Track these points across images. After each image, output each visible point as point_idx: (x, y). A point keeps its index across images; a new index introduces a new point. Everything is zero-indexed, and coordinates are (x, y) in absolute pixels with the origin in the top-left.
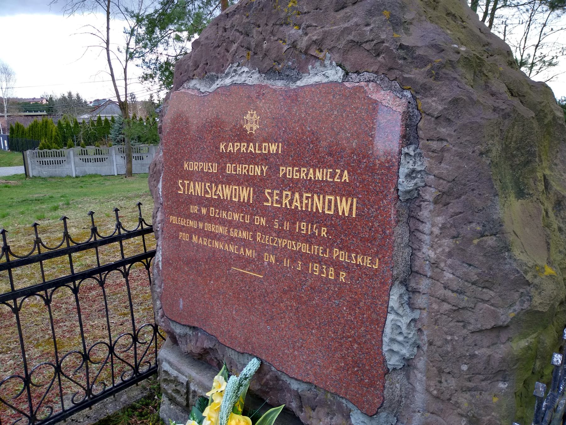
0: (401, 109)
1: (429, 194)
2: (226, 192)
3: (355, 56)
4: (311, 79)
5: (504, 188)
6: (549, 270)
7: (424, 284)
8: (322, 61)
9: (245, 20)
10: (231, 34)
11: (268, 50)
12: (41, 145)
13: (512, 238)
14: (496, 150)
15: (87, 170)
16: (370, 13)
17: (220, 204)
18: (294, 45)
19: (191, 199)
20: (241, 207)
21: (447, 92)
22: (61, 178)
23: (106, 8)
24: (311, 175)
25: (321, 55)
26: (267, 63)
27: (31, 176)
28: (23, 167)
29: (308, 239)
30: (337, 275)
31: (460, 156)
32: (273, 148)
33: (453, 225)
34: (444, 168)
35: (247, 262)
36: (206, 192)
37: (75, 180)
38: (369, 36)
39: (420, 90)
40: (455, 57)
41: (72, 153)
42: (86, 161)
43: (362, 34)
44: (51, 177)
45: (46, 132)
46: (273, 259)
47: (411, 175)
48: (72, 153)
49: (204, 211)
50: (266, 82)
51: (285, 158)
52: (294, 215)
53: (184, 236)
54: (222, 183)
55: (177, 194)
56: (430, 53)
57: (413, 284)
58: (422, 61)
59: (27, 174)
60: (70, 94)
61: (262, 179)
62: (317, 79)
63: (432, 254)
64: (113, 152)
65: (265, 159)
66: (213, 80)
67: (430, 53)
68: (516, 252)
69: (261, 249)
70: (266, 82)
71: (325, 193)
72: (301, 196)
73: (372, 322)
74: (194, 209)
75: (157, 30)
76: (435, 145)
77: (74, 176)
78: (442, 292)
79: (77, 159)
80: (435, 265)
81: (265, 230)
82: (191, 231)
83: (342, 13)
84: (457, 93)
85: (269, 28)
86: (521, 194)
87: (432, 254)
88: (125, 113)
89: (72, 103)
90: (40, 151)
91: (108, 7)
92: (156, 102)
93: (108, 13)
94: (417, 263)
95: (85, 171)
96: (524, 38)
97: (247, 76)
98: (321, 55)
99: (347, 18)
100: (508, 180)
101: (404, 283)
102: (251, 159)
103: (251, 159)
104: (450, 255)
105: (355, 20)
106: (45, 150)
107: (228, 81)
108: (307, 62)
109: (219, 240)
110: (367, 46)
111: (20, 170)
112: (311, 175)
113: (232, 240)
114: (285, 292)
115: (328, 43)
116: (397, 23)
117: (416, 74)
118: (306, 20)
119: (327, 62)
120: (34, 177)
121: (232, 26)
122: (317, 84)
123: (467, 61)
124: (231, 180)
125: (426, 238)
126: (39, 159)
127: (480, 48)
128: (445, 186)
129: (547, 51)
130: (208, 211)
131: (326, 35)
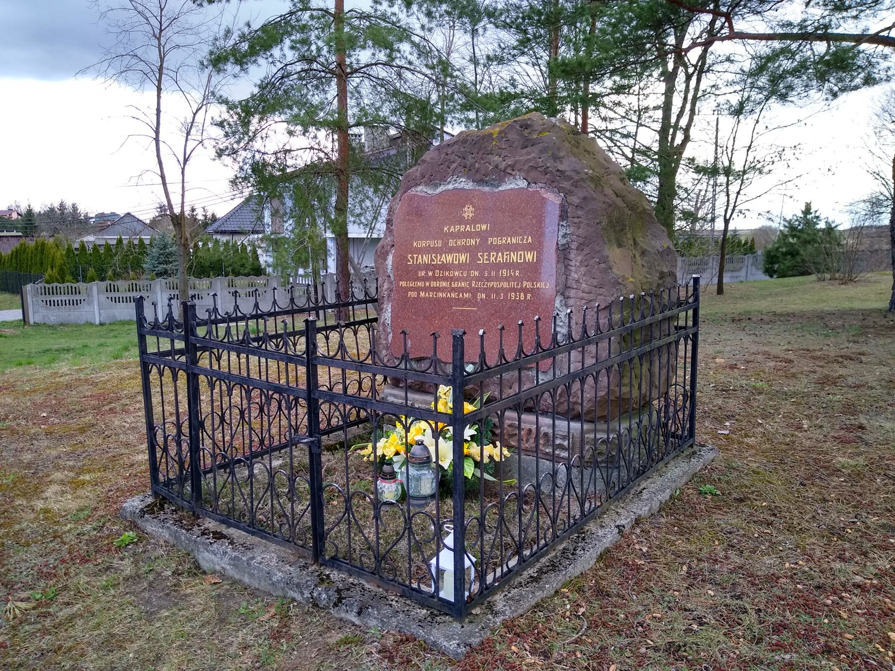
0: (558, 202)
1: (574, 246)
2: (449, 258)
3: (533, 174)
4: (509, 185)
5: (610, 240)
6: (631, 279)
7: (572, 293)
8: (514, 176)
9: (462, 150)
10: (452, 157)
11: (479, 168)
12: (47, 277)
13: (612, 263)
14: (605, 222)
15: (117, 314)
16: (541, 152)
17: (444, 267)
18: (497, 167)
19: (419, 267)
20: (460, 267)
21: (581, 193)
22: (78, 325)
23: (156, 83)
24: (509, 241)
25: (514, 173)
26: (478, 176)
27: (32, 322)
28: (20, 311)
29: (507, 279)
30: (526, 296)
31: (588, 225)
32: (484, 227)
33: (586, 260)
34: (581, 232)
35: (465, 302)
36: (432, 260)
37: (99, 328)
38: (541, 164)
39: (568, 193)
40: (585, 177)
41: (95, 289)
42: (116, 300)
43: (537, 163)
44: (62, 324)
45: (41, 259)
46: (484, 296)
47: (564, 236)
48: (95, 289)
49: (430, 274)
50: (477, 188)
51: (491, 233)
52: (498, 266)
53: (413, 294)
54: (445, 253)
55: (406, 265)
56: (573, 174)
57: (567, 294)
58: (569, 178)
59: (25, 320)
60: (62, 205)
61: (476, 247)
62: (512, 186)
63: (576, 276)
64: (158, 288)
65: (478, 234)
66: (436, 186)
67: (573, 174)
68: (615, 270)
69: (474, 291)
70: (477, 188)
71: (518, 250)
72: (503, 254)
73: (546, 318)
74: (422, 274)
75: (255, 120)
76: (576, 220)
77: (97, 322)
78: (581, 295)
79: (103, 297)
80: (577, 281)
81: (478, 279)
82: (418, 290)
83: (525, 150)
84: (586, 194)
85: (480, 155)
86: (620, 246)
87: (576, 276)
88: (180, 230)
89: (64, 219)
90: (47, 286)
91: (159, 81)
92: (200, 217)
93: (159, 90)
94: (569, 282)
95: (114, 316)
96: (732, 138)
97: (464, 184)
98: (514, 173)
99: (529, 153)
100: (612, 237)
101: (563, 294)
102: (468, 235)
103: (468, 235)
104: (584, 275)
105: (533, 155)
106: (55, 284)
107: (450, 187)
108: (505, 176)
109: (442, 291)
110: (540, 169)
111: (16, 314)
112: (509, 241)
113: (453, 290)
114: (492, 315)
115: (518, 166)
116: (555, 158)
117: (566, 185)
118: (504, 153)
119: (517, 177)
120: (36, 325)
121: (453, 152)
122: (512, 189)
123: (592, 179)
124: (451, 250)
125: (573, 269)
126: (44, 298)
127: (603, 171)
128: (581, 240)
129: (761, 153)
130: (434, 273)
131: (516, 162)
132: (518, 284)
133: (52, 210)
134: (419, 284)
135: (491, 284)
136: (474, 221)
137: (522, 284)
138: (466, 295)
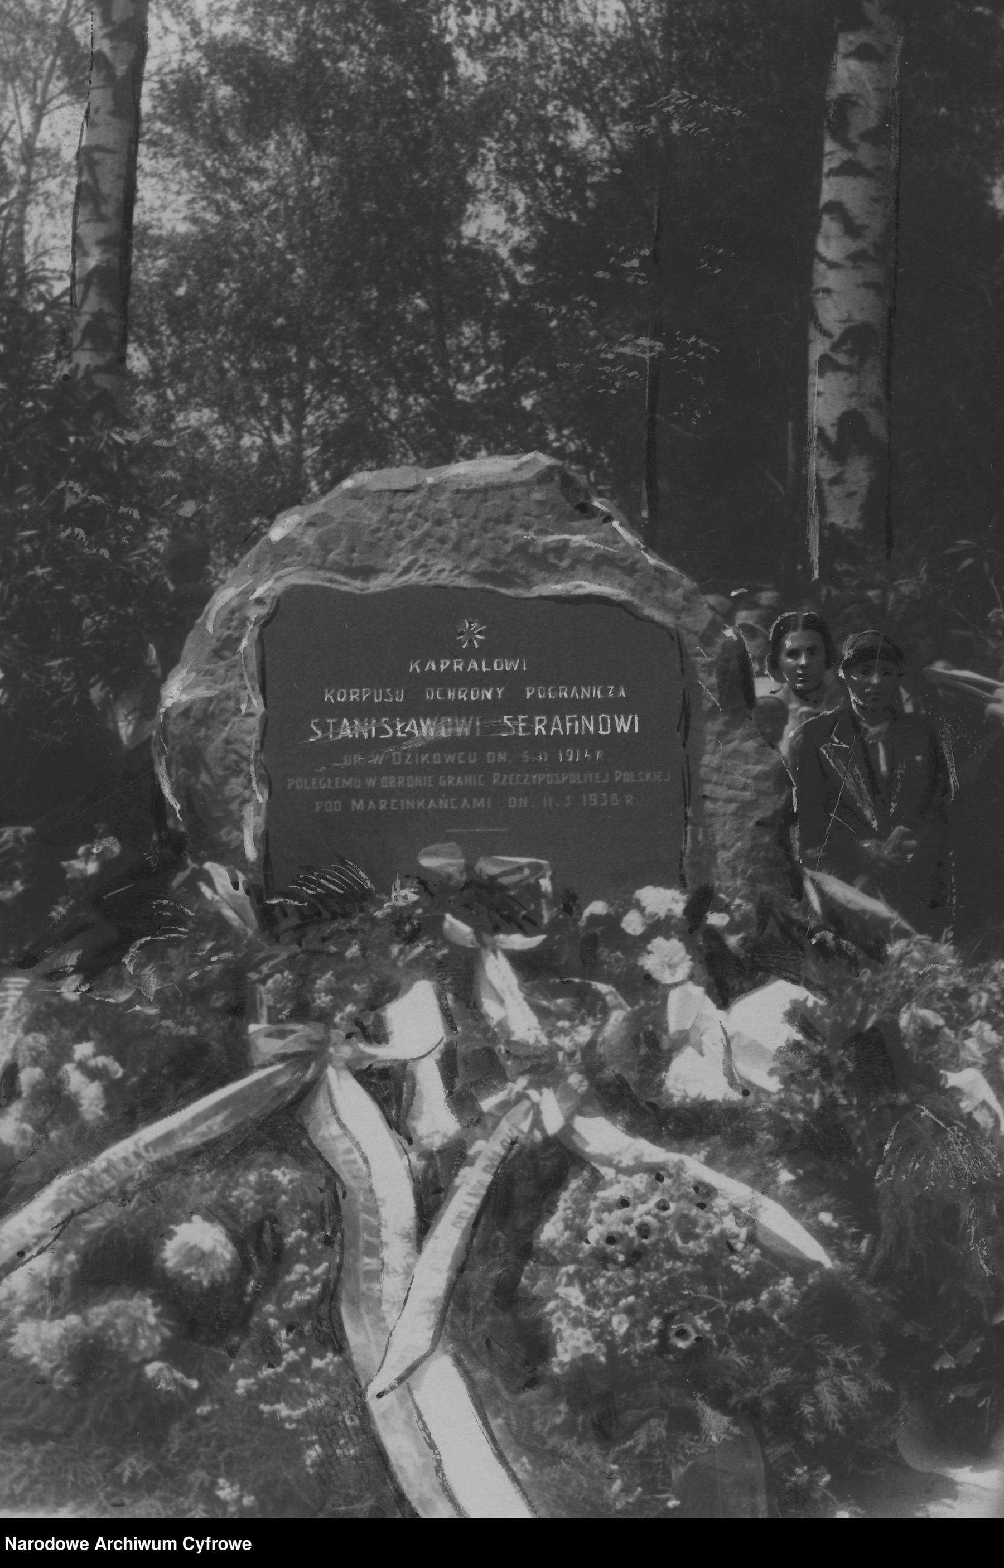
51: (536, 676)
103: (479, 680)
132: (602, 776)
133: (490, 454)
134: (348, 783)
135: (538, 778)
136: (486, 652)
137: (612, 776)
138: (479, 803)
